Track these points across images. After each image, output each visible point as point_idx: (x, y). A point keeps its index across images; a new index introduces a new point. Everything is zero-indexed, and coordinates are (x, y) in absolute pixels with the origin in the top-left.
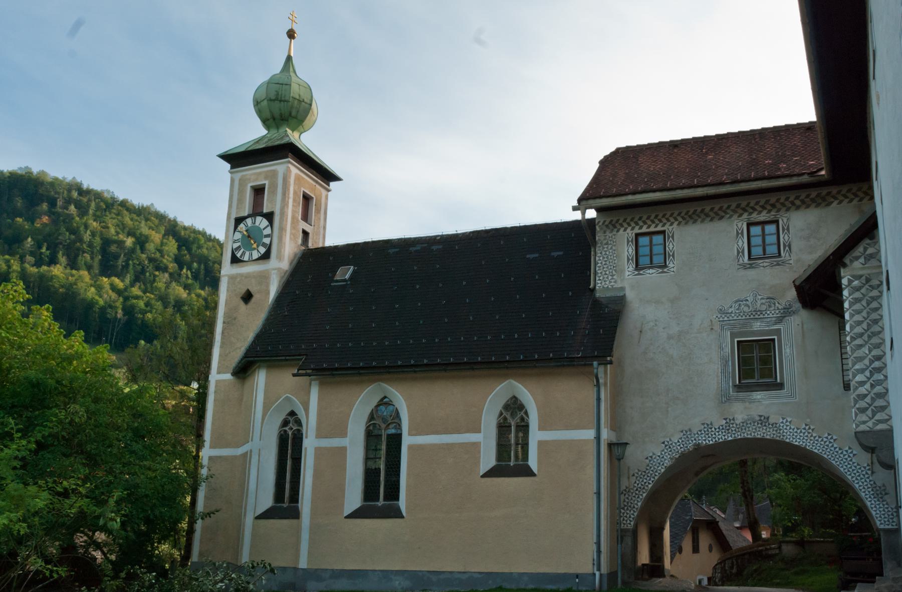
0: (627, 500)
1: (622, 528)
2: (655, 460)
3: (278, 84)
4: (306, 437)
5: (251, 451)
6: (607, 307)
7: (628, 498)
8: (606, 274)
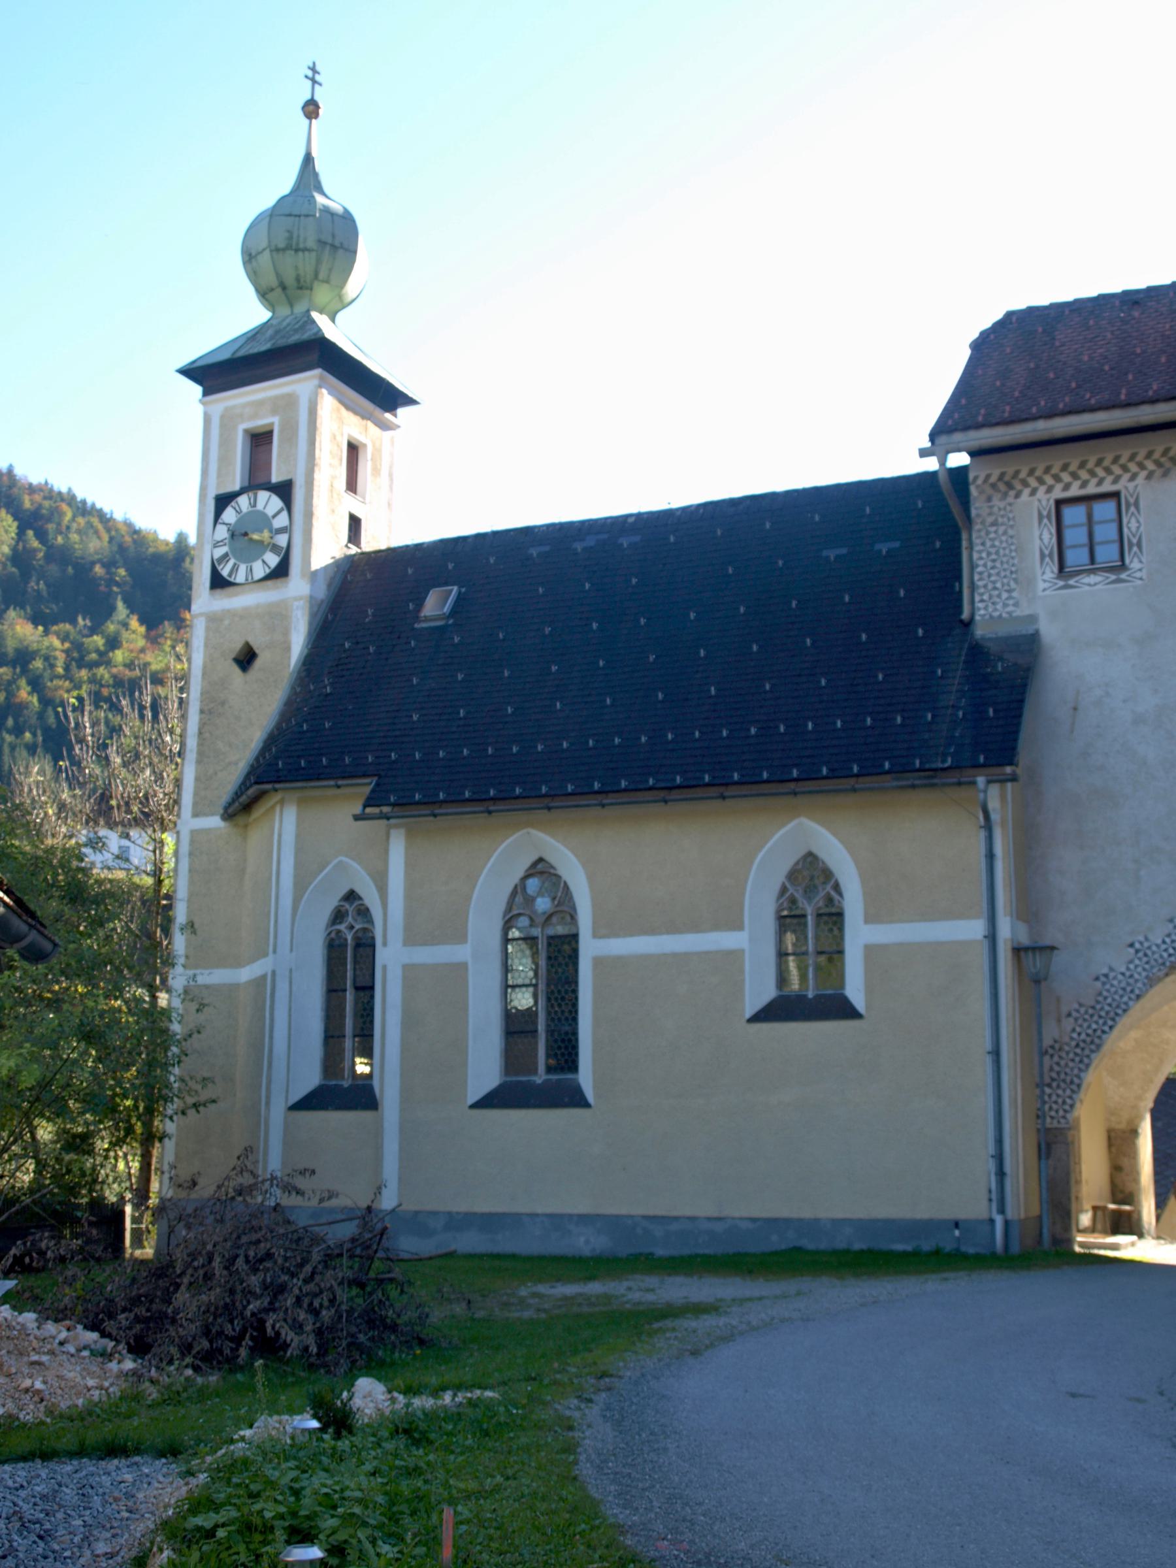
0: (1056, 1068)
1: (1048, 1126)
2: (1115, 983)
3: (290, 215)
4: (385, 944)
5: (274, 973)
6: (1001, 659)
7: (1058, 1064)
8: (995, 588)
